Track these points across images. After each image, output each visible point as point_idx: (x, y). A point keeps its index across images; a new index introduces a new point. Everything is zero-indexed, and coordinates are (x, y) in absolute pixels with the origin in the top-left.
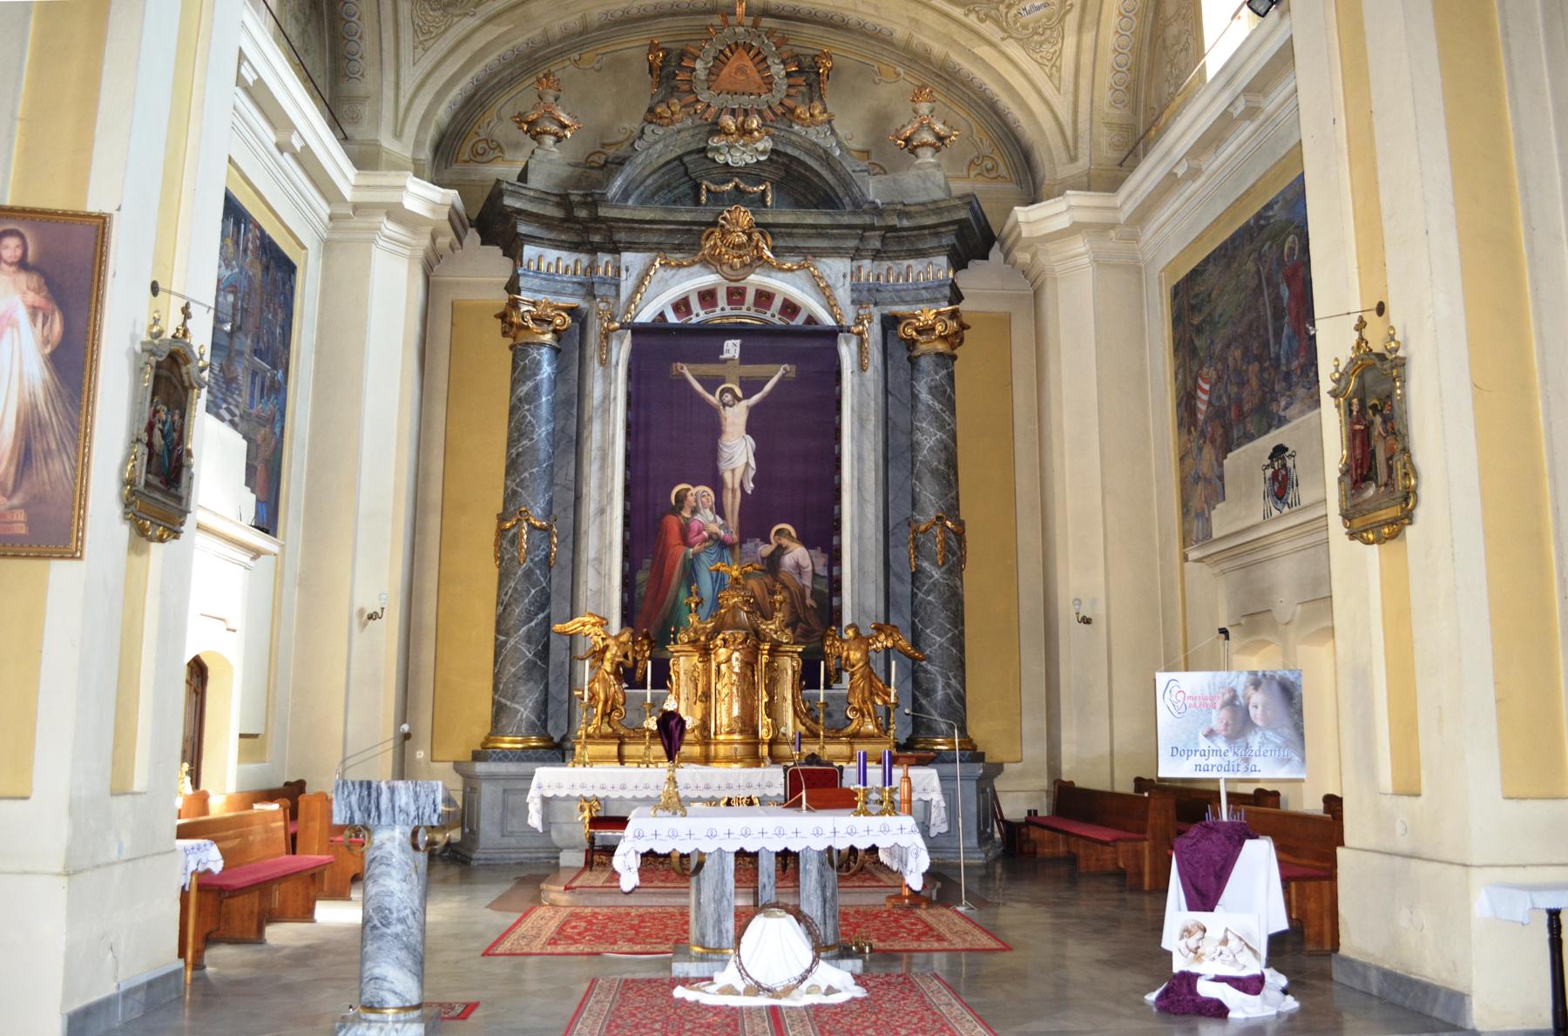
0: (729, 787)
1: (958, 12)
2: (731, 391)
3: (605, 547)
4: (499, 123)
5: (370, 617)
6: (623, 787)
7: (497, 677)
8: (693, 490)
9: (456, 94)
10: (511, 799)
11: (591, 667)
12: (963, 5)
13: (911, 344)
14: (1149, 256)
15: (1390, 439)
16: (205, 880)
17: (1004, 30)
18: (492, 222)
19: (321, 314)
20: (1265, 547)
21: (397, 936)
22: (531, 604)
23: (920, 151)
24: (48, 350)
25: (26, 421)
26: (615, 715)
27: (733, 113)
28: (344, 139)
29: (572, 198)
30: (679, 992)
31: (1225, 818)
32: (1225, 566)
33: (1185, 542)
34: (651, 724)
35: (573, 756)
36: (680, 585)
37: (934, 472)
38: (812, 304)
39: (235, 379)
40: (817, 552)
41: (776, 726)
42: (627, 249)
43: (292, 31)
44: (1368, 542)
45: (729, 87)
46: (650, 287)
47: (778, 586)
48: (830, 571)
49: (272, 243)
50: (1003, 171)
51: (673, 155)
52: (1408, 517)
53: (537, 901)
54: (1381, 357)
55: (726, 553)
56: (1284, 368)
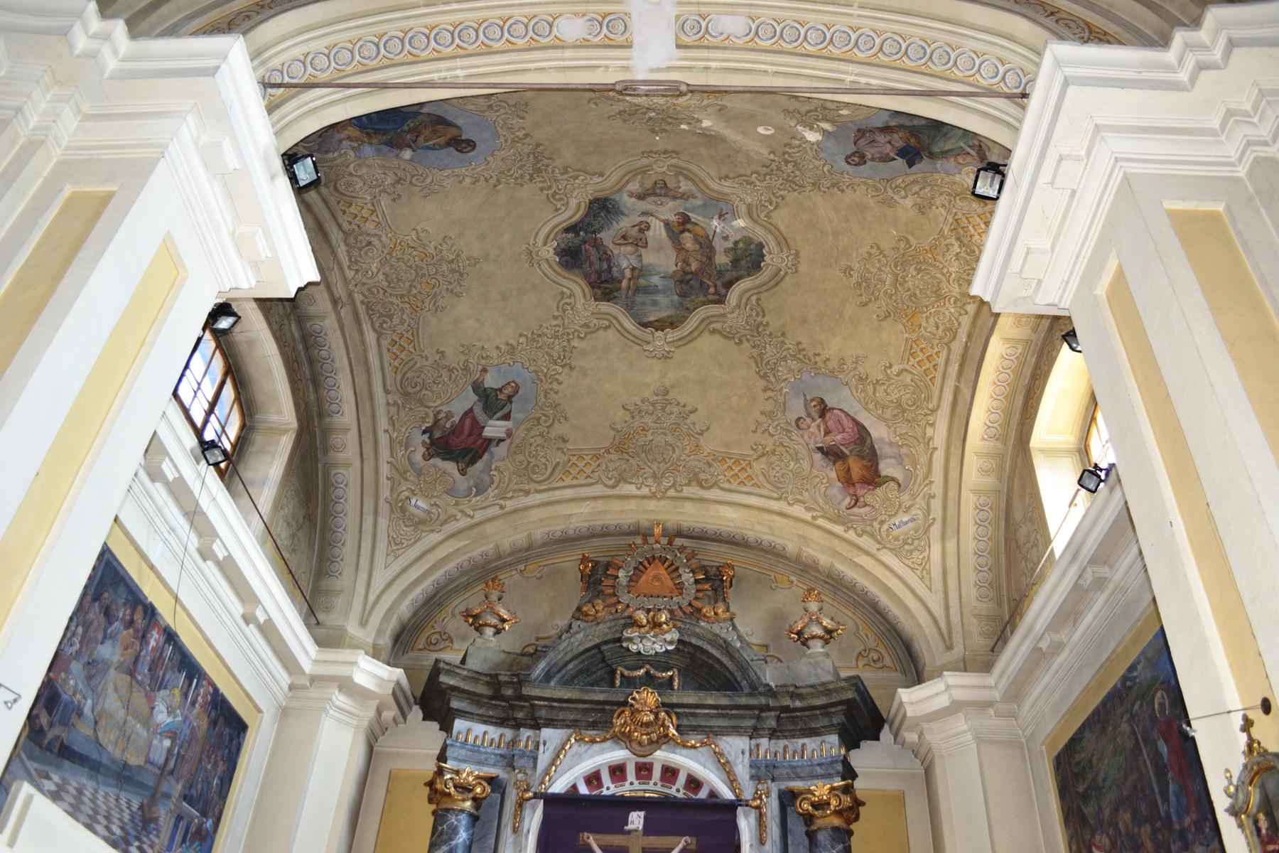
1: (839, 529)
4: (453, 623)
9: (417, 593)
12: (842, 524)
17: (879, 543)
18: (433, 700)
23: (811, 643)
29: (501, 678)
39: (156, 820)
43: (282, 532)
50: (888, 661)
51: (592, 644)
56: (1177, 827)
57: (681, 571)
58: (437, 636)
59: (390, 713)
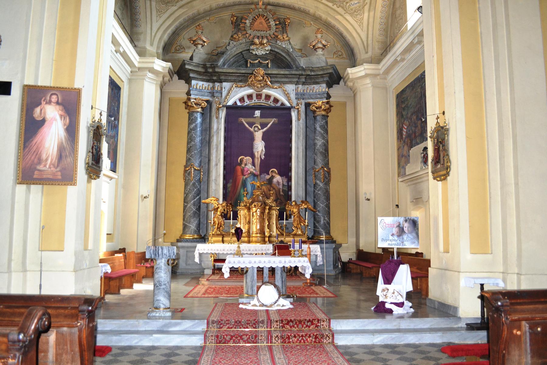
0: (256, 250)
1: (330, 4)
2: (257, 127)
3: (218, 176)
4: (184, 40)
5: (145, 198)
6: (224, 250)
7: (184, 216)
8: (245, 158)
9: (170, 31)
10: (189, 254)
11: (214, 213)
12: (332, 2)
13: (314, 112)
14: (390, 84)
15: (444, 152)
16: (107, 275)
18: (182, 73)
19: (128, 103)
20: (420, 178)
21: (164, 289)
22: (195, 193)
23: (318, 50)
24: (65, 127)
25: (60, 147)
26: (221, 228)
27: (258, 37)
28: (135, 46)
30: (241, 306)
31: (395, 258)
32: (409, 183)
33: (399, 175)
34: (233, 231)
35: (208, 241)
36: (241, 188)
37: (321, 153)
38: (283, 99)
40: (284, 178)
41: (270, 230)
42: (225, 82)
43: (119, 13)
44: (438, 181)
45: (257, 29)
46: (232, 93)
47: (271, 189)
48: (288, 184)
49: (114, 81)
50: (344, 56)
51: (239, 51)
52: (448, 174)
53: (198, 284)
54: (442, 128)
55: (256, 178)
57: (270, 20)
58: (179, 47)
59: (167, 78)
